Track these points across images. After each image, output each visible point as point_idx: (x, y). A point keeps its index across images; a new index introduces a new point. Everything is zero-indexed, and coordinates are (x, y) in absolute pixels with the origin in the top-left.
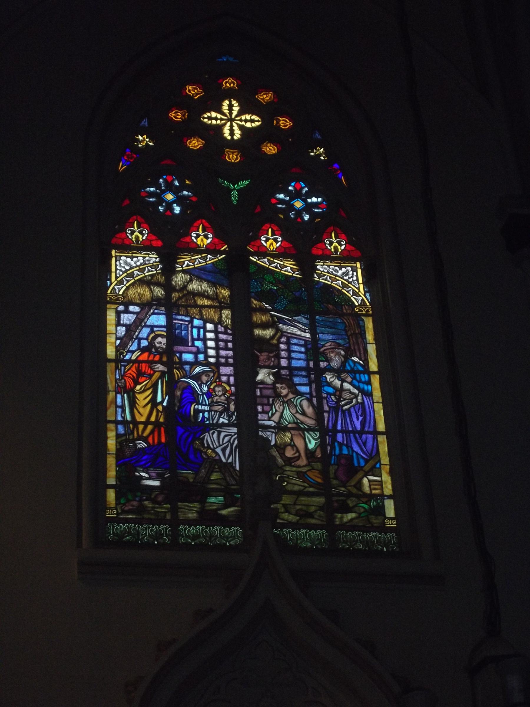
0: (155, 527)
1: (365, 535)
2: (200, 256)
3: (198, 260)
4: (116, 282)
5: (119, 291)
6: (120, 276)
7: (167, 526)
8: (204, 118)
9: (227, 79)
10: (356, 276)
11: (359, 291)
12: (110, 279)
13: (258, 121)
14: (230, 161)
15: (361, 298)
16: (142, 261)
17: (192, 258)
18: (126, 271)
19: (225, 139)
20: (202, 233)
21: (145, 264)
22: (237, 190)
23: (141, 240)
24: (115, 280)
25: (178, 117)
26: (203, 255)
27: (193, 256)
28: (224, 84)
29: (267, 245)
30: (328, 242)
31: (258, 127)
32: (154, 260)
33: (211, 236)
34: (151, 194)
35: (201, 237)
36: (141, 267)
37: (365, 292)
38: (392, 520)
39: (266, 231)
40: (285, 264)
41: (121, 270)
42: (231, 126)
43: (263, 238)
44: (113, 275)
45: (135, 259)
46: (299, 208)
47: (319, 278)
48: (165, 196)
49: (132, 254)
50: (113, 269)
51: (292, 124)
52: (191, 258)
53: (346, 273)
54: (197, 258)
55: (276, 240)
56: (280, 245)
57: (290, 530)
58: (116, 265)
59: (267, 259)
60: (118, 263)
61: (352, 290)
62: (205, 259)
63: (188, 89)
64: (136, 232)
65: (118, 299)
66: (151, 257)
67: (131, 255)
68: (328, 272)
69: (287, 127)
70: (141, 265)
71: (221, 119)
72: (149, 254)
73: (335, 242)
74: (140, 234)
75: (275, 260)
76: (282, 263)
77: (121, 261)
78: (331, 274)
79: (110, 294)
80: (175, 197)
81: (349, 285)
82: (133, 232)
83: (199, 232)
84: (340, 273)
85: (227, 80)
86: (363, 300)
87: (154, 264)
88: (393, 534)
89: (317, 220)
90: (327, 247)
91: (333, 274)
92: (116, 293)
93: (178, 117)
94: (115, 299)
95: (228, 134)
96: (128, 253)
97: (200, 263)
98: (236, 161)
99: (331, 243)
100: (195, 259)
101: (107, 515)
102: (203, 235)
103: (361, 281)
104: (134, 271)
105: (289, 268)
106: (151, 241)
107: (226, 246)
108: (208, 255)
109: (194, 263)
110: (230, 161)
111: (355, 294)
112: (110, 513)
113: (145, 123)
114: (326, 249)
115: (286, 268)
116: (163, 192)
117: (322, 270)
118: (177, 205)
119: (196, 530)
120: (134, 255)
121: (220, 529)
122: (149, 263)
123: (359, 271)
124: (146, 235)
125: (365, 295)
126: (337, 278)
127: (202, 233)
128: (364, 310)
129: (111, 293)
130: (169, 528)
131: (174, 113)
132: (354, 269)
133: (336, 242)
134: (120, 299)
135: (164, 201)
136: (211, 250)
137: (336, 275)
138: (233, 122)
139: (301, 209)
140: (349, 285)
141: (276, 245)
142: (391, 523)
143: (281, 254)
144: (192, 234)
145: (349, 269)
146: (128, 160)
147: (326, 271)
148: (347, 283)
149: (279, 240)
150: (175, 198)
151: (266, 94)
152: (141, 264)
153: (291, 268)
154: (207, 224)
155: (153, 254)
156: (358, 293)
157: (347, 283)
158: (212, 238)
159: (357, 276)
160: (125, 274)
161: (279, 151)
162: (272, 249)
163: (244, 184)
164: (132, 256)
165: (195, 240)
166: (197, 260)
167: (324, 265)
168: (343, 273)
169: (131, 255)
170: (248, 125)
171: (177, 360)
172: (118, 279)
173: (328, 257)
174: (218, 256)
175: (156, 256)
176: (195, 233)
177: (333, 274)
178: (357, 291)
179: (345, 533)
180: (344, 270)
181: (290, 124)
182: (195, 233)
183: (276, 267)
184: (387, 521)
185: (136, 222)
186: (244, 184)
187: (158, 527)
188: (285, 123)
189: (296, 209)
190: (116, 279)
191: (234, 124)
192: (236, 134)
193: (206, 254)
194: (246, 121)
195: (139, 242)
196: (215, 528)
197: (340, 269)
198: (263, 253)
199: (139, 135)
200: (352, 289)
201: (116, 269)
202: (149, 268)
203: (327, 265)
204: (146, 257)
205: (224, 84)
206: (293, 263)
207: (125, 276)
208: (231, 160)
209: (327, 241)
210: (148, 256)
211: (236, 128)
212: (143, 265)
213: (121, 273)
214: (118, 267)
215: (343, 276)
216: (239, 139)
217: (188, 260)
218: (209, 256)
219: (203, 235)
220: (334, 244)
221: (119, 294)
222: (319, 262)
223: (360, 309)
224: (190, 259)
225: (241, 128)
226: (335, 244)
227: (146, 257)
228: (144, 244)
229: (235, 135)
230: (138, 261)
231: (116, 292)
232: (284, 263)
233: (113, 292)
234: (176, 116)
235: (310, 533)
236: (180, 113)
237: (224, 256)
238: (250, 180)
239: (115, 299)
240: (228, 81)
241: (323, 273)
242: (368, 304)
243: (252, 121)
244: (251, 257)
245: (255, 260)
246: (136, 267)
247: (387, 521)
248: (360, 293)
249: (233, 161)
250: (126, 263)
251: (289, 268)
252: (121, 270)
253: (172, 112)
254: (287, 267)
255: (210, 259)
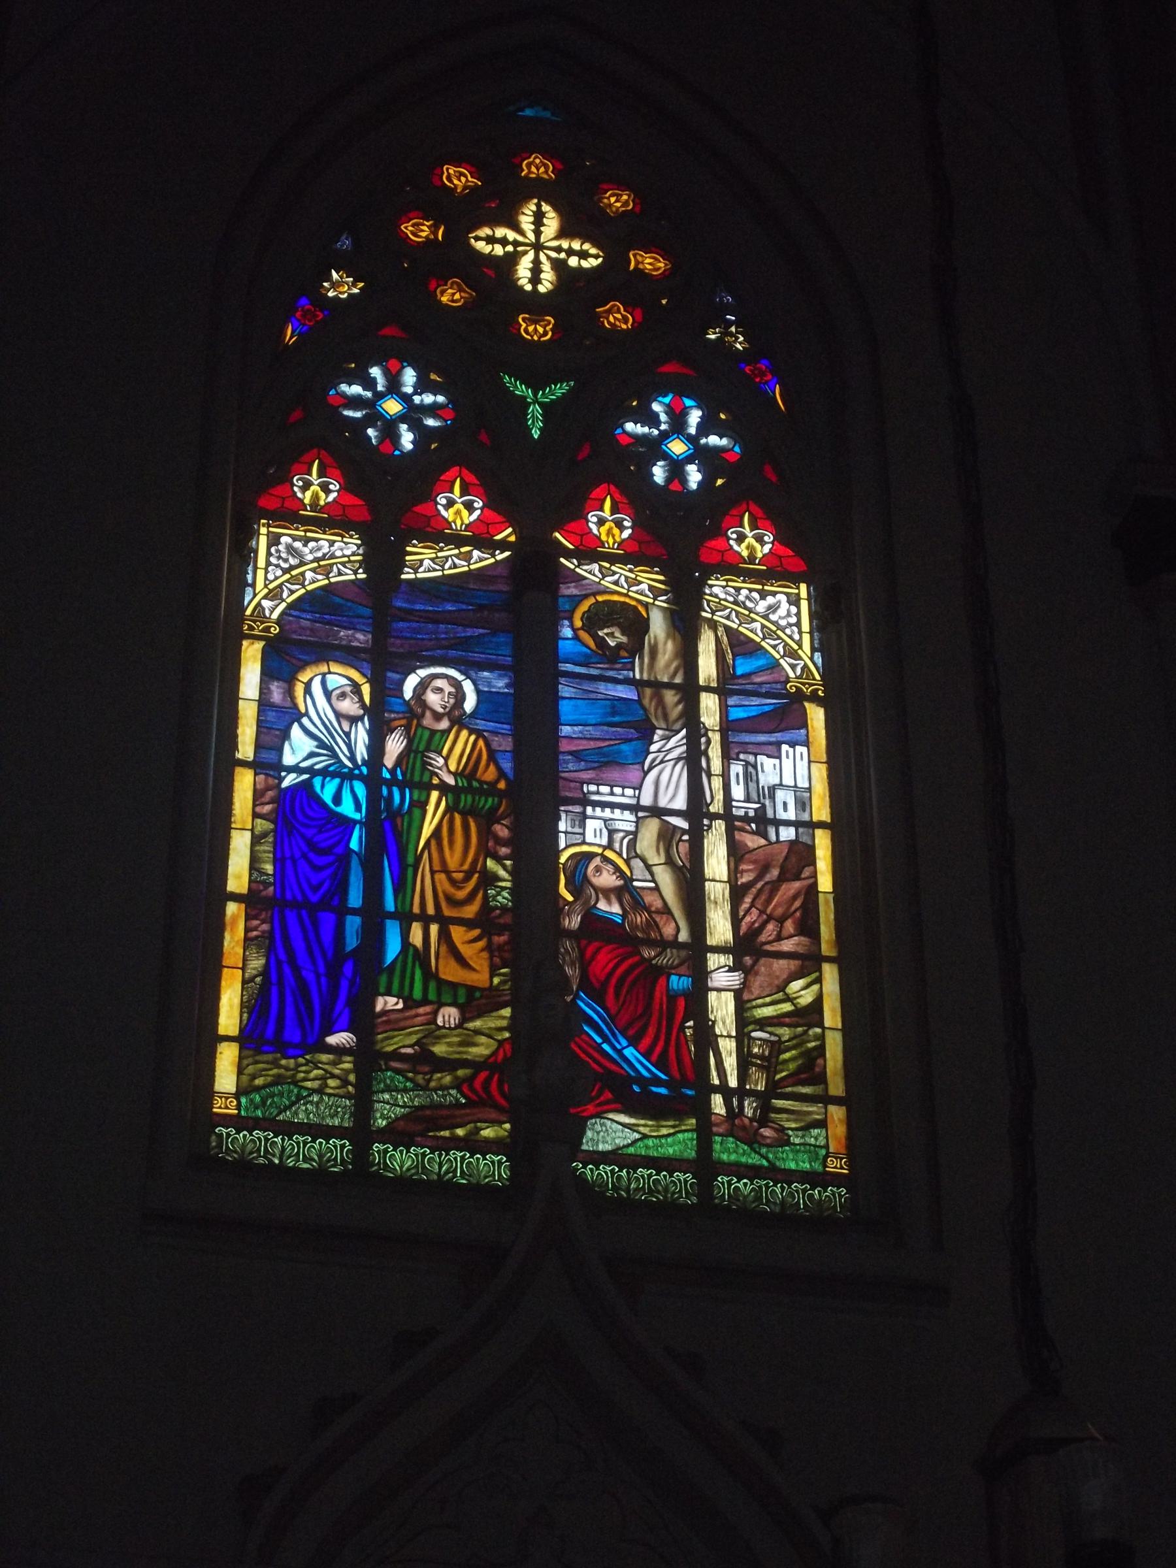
0: (241, 1135)
1: (740, 1185)
2: (456, 551)
3: (452, 560)
4: (266, 591)
5: (271, 612)
6: (276, 578)
7: (308, 1139)
8: (477, 239)
9: (529, 157)
10: (795, 615)
11: (800, 647)
12: (253, 585)
13: (596, 257)
14: (529, 337)
15: (803, 662)
16: (325, 550)
17: (440, 554)
18: (292, 568)
19: (521, 289)
20: (612, 515)
21: (333, 557)
22: (541, 405)
23: (322, 503)
24: (263, 586)
25: (651, 261)
26: (464, 550)
27: (441, 550)
28: (525, 168)
29: (449, 515)
30: (595, 519)
31: (593, 270)
32: (355, 548)
33: (335, 486)
34: (355, 402)
35: (607, 525)
36: (322, 563)
37: (813, 650)
38: (227, 1098)
39: (306, 466)
40: (638, 578)
41: (277, 566)
42: (536, 262)
43: (592, 518)
44: (260, 574)
45: (312, 544)
46: (678, 456)
47: (713, 613)
48: (686, 448)
49: (305, 531)
50: (261, 562)
51: (402, 227)
52: (436, 553)
53: (773, 608)
54: (451, 556)
55: (469, 507)
56: (479, 518)
57: (269, 1135)
58: (269, 554)
59: (599, 565)
60: (273, 550)
61: (783, 644)
62: (467, 557)
63: (446, 174)
64: (457, 503)
65: (267, 629)
66: (346, 543)
67: (302, 534)
68: (736, 603)
69: (660, 272)
70: (323, 558)
71: (516, 244)
72: (343, 536)
73: (750, 535)
74: (757, 542)
75: (613, 568)
76: (633, 576)
77: (281, 547)
78: (740, 606)
79: (251, 616)
80: (691, 447)
81: (779, 632)
82: (307, 486)
83: (603, 511)
84: (762, 607)
85: (531, 160)
86: (805, 666)
87: (352, 558)
88: (465, 1155)
89: (433, 447)
90: (295, 493)
91: (746, 608)
92: (265, 617)
93: (651, 261)
94: (260, 628)
95: (527, 280)
96: (297, 529)
97: (455, 566)
98: (542, 339)
99: (741, 538)
100: (447, 558)
101: (215, 1110)
102: (462, 503)
103: (806, 626)
104: (305, 571)
105: (644, 587)
106: (488, 524)
107: (510, 530)
108: (472, 550)
109: (629, 587)
110: (529, 337)
111: (793, 654)
112: (222, 1106)
113: (345, 243)
114: (589, 533)
115: (638, 585)
116: (379, 396)
117: (722, 596)
118: (409, 429)
119: (599, 1174)
120: (309, 534)
121: (685, 1179)
122: (344, 556)
123: (804, 605)
124: (335, 494)
125: (812, 659)
126: (752, 615)
127: (612, 514)
128: (258, 627)
129: (252, 615)
130: (505, 1162)
131: (413, 226)
132: (795, 601)
133: (753, 537)
134: (272, 629)
135: (381, 416)
136: (480, 538)
137: (750, 610)
138: (541, 252)
139: (683, 459)
140: (779, 632)
141: (469, 518)
142: (838, 1166)
143: (632, 555)
144: (438, 499)
145: (783, 598)
146: (303, 322)
147: (731, 599)
148: (774, 628)
149: (331, 487)
150: (691, 451)
151: (617, 195)
152: (324, 555)
153: (651, 588)
154: (471, 478)
155: (351, 537)
156: (796, 651)
157: (774, 628)
158: (482, 509)
159: (798, 614)
160: (287, 576)
161: (636, 324)
162: (459, 528)
163: (559, 390)
164: (305, 536)
165: (300, 495)
166: (450, 559)
167: (727, 586)
168: (770, 607)
169: (302, 534)
170: (573, 262)
171: (388, 776)
172: (271, 586)
173: (732, 567)
174: (498, 552)
175: (359, 542)
176: (445, 497)
177: (746, 608)
178: (796, 647)
179: (655, 1175)
180: (770, 600)
181: (666, 265)
182: (445, 497)
183: (616, 583)
184: (831, 1161)
185: (317, 461)
186: (559, 390)
187: (749, 1182)
188: (650, 263)
189: (672, 456)
190: (266, 586)
191: (543, 258)
192: (543, 281)
193: (471, 548)
194: (570, 252)
195: (757, 561)
196: (601, 1168)
197: (763, 597)
198: (590, 551)
199: (333, 270)
200: (783, 641)
201: (268, 564)
202: (340, 566)
203: (733, 587)
204: (335, 541)
205: (525, 168)
206: (661, 578)
207: (287, 581)
208: (532, 336)
209: (297, 481)
210: (340, 538)
211: (546, 266)
212: (327, 559)
213: (279, 573)
214: (273, 560)
215: (769, 614)
216: (550, 293)
217: (429, 559)
218: (476, 553)
219: (462, 503)
220: (747, 541)
221: (270, 618)
222: (717, 579)
223: (251, 625)
224: (434, 555)
225: (559, 266)
226: (750, 540)
227: (335, 541)
228: (331, 514)
229: (541, 283)
230: (319, 549)
231: (264, 614)
232: (637, 576)
233: (259, 612)
234: (419, 231)
235: (276, 1139)
236: (427, 226)
237: (507, 554)
238: (572, 383)
239: (260, 628)
240: (533, 161)
241: (722, 602)
242: (818, 677)
243: (583, 255)
244: (562, 560)
245: (572, 567)
246: (312, 562)
247: (831, 1161)
248: (800, 652)
249: (536, 338)
250: (290, 549)
251: (644, 587)
252: (277, 566)
253: (408, 222)
254: (640, 583)
255: (480, 559)
